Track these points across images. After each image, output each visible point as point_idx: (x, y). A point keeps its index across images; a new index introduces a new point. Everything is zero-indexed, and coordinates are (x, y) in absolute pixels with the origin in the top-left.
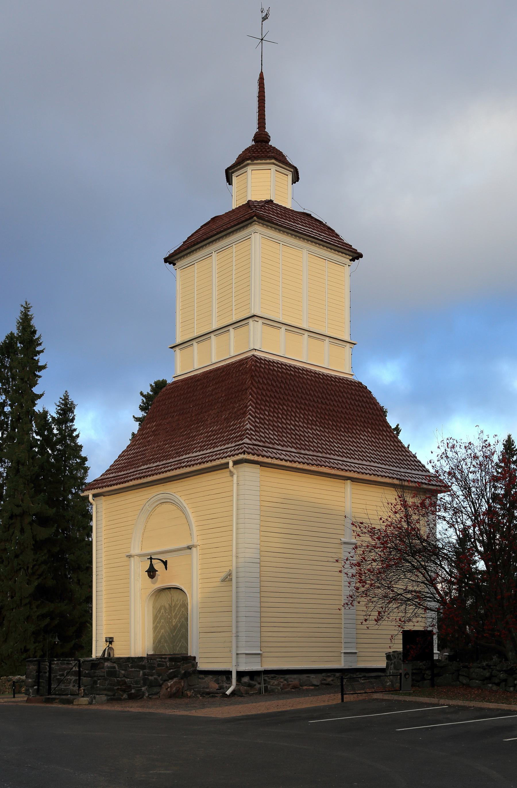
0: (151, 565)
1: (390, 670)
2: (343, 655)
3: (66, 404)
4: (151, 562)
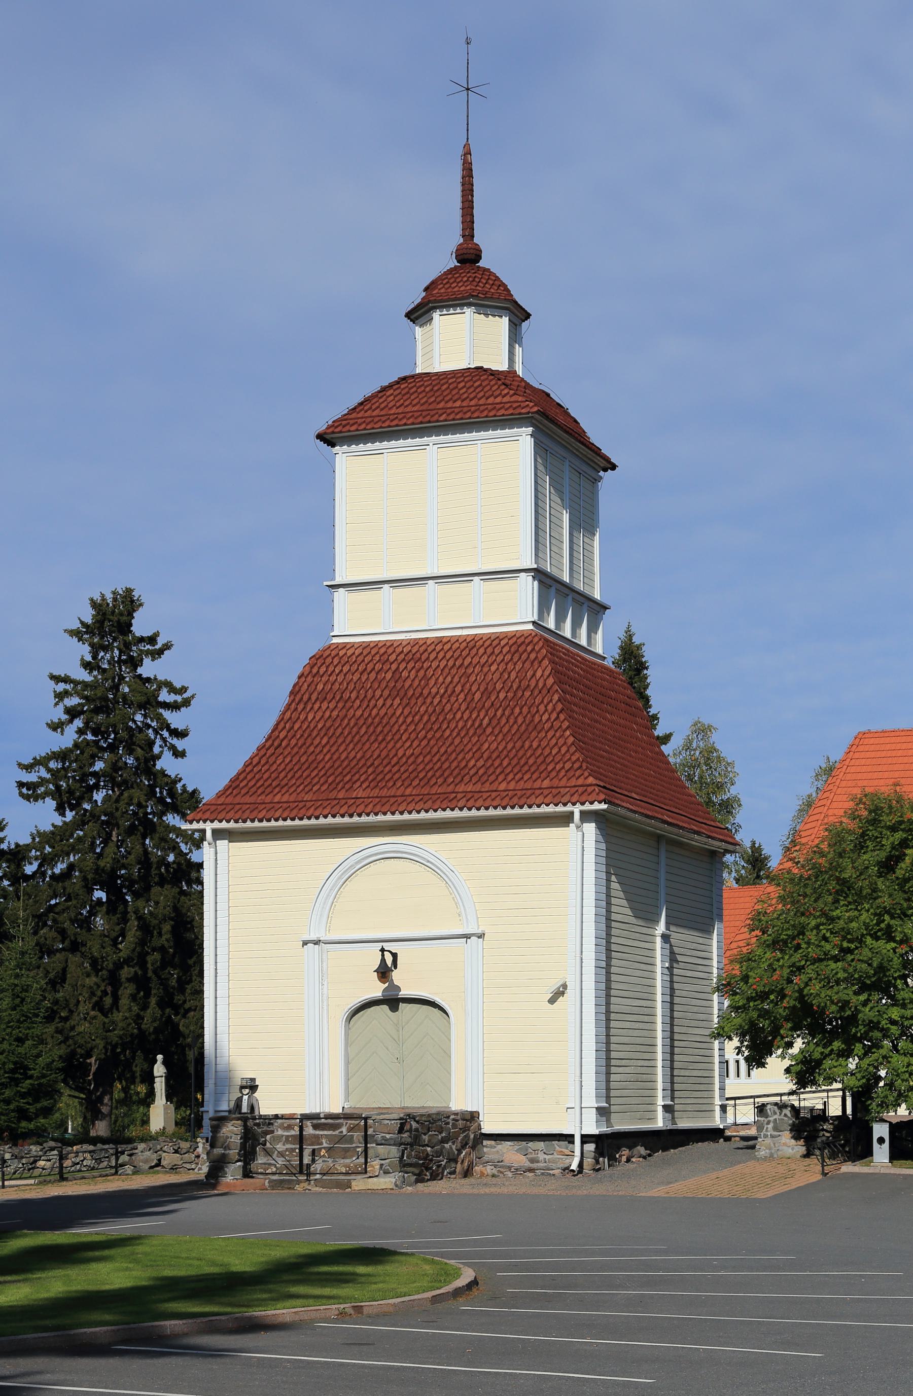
0: (383, 960)
4: (383, 955)
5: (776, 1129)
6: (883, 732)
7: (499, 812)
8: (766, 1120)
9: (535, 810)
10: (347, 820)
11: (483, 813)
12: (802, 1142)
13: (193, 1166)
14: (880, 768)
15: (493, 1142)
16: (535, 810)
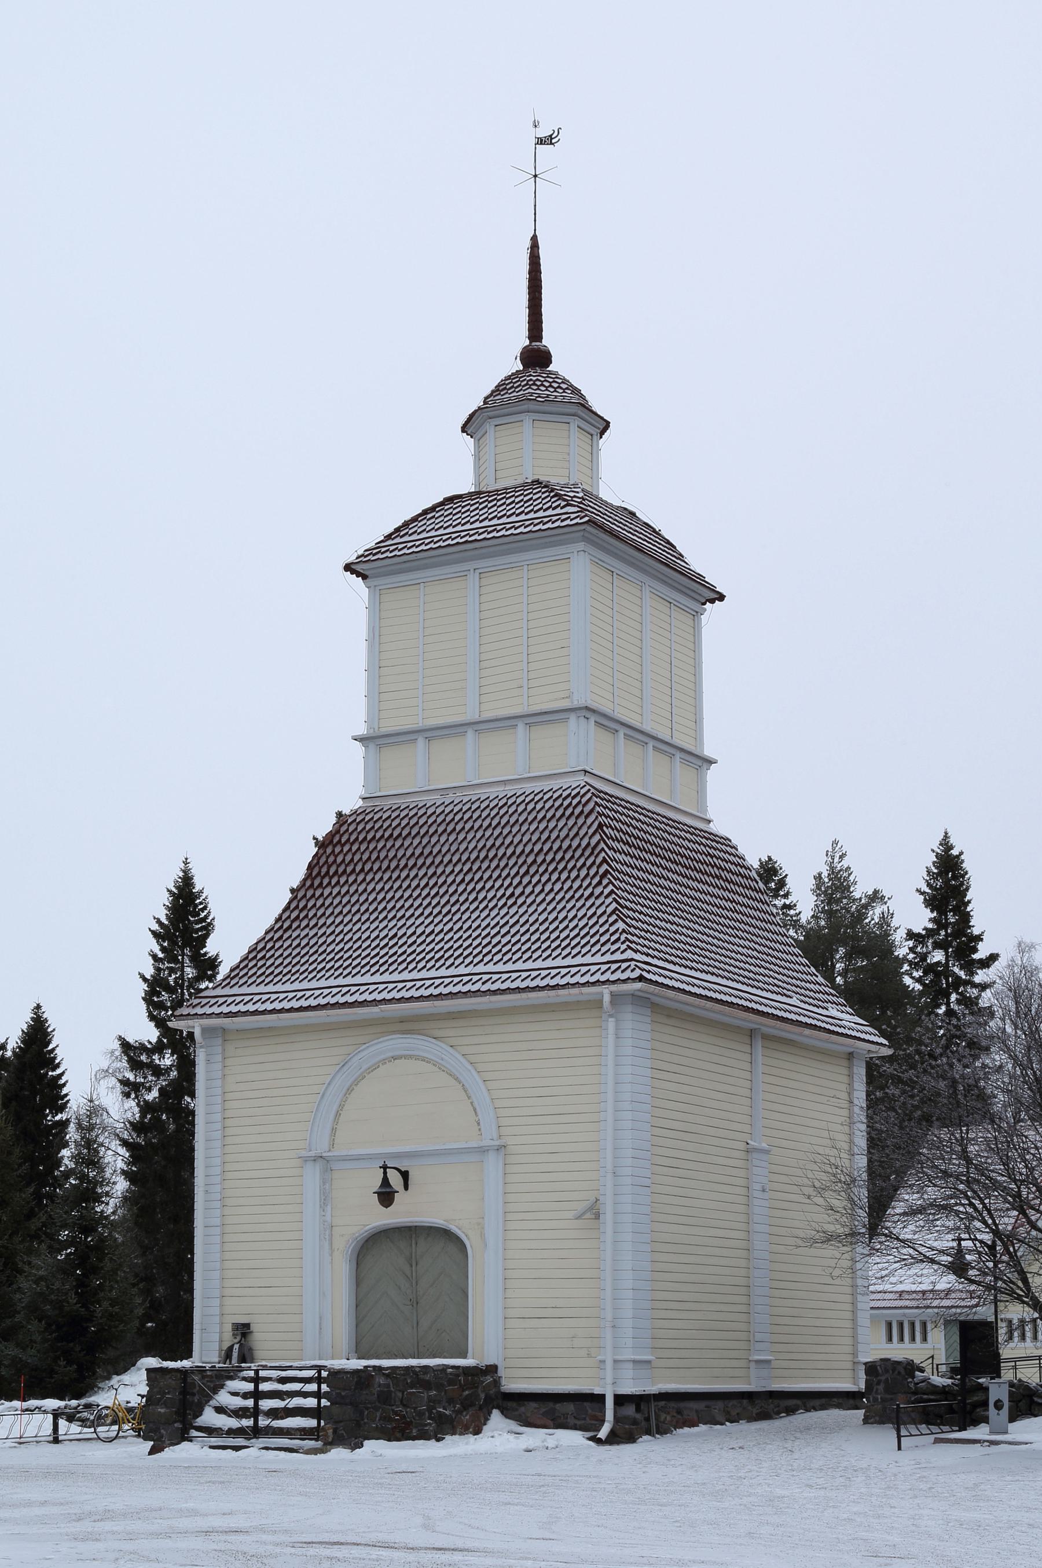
0: (385, 1182)
1: (876, 1392)
2: (753, 1365)
3: (834, 874)
4: (385, 1173)
15: (514, 1405)
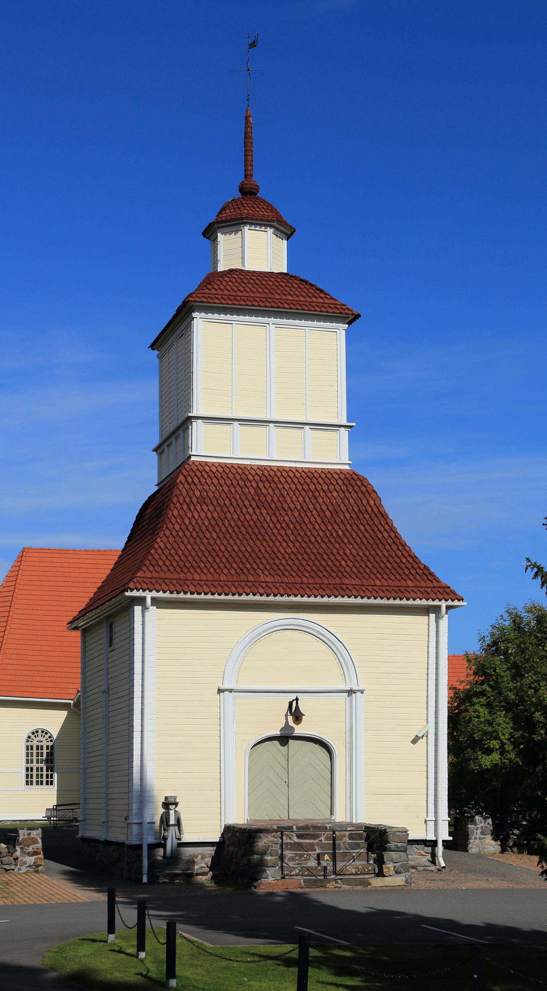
5: (483, 833)
6: (40, 549)
7: (384, 601)
8: (475, 827)
9: (411, 602)
10: (264, 598)
11: (365, 601)
12: (499, 843)
13: (13, 867)
14: (46, 574)
16: (411, 602)
